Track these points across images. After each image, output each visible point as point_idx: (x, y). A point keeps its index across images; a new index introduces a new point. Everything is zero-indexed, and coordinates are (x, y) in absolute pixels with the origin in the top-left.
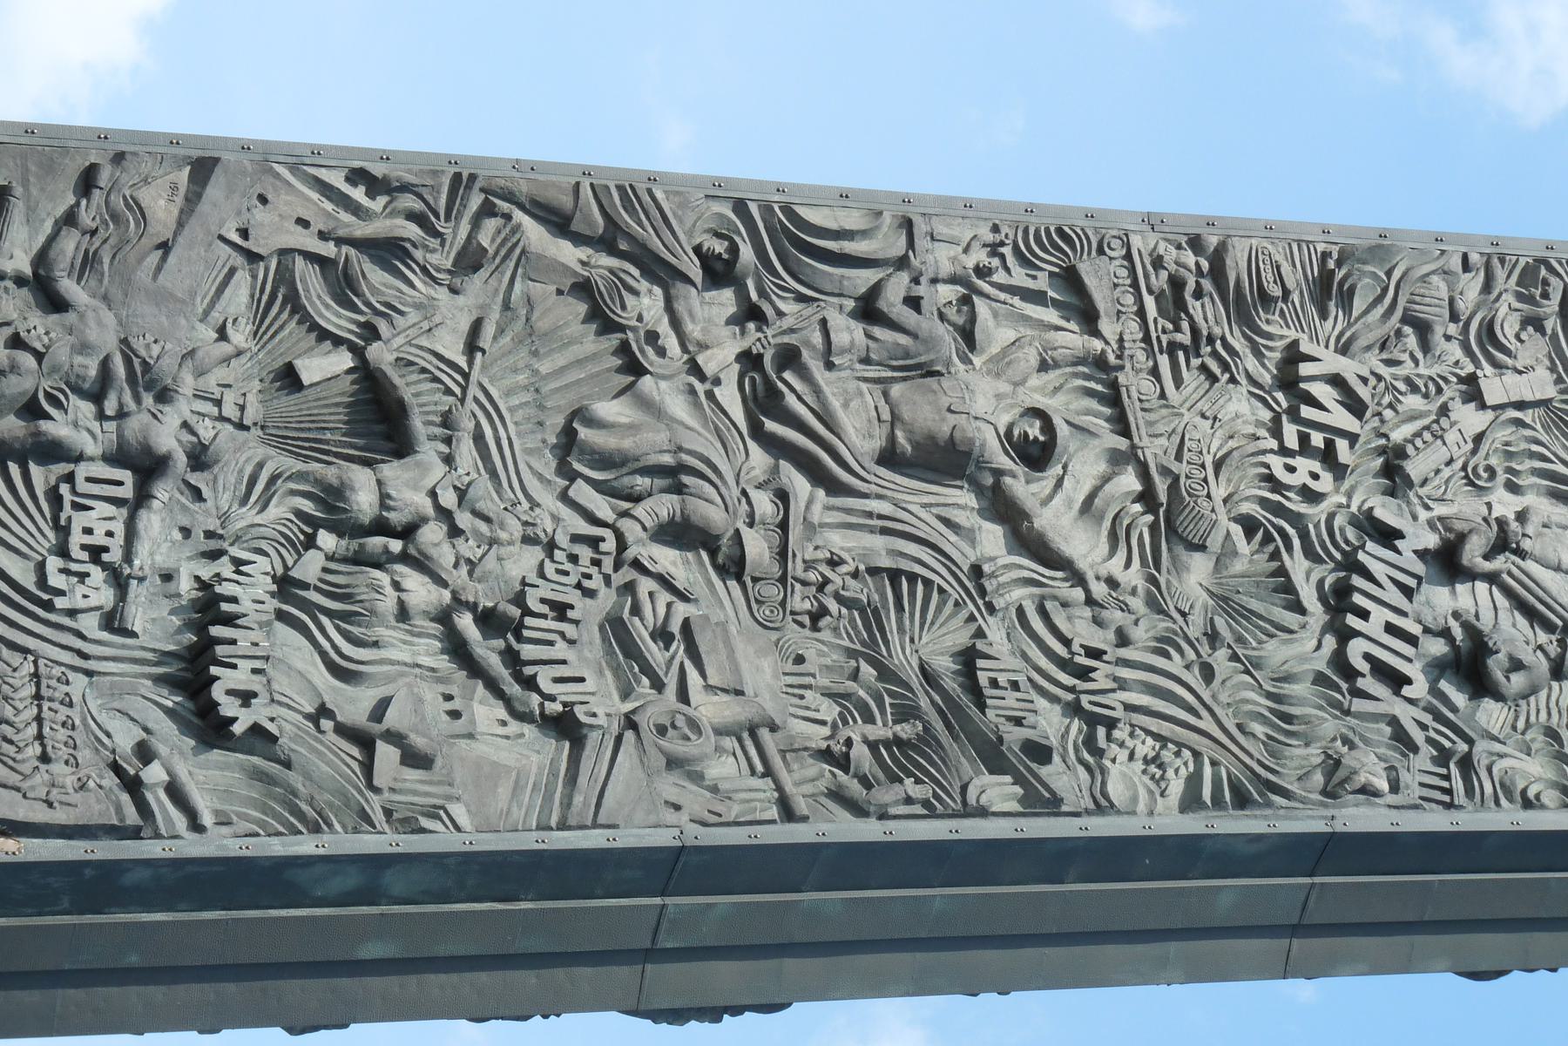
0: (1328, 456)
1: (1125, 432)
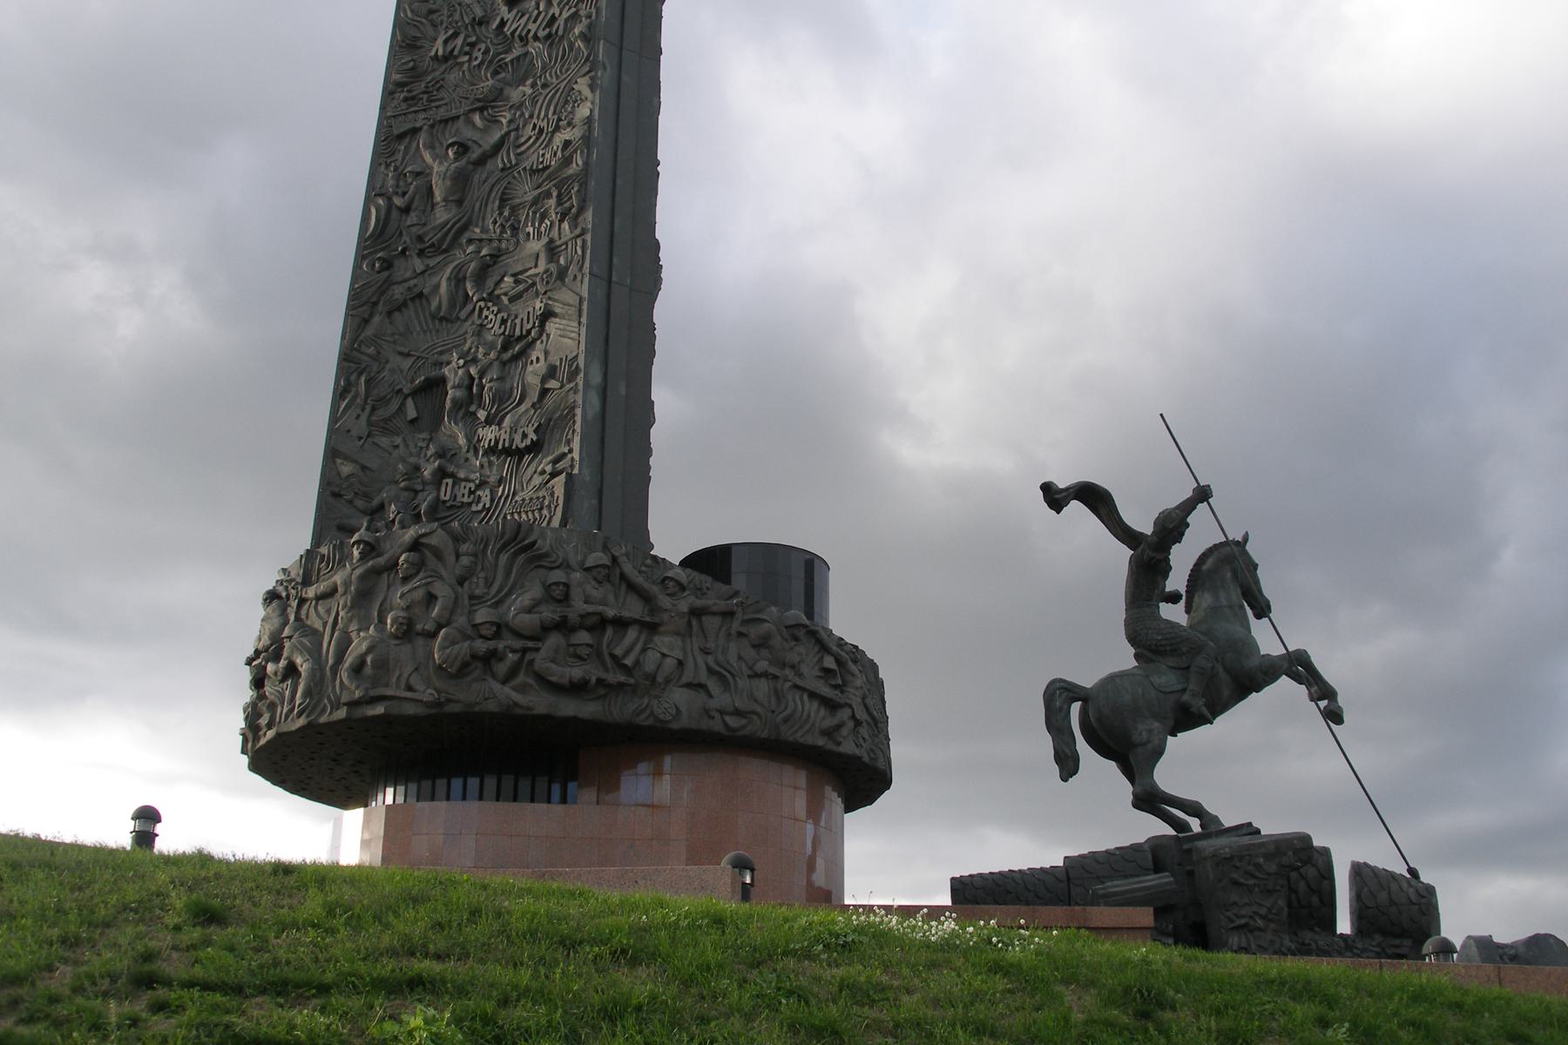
0: (472, 45)
1: (458, 117)
